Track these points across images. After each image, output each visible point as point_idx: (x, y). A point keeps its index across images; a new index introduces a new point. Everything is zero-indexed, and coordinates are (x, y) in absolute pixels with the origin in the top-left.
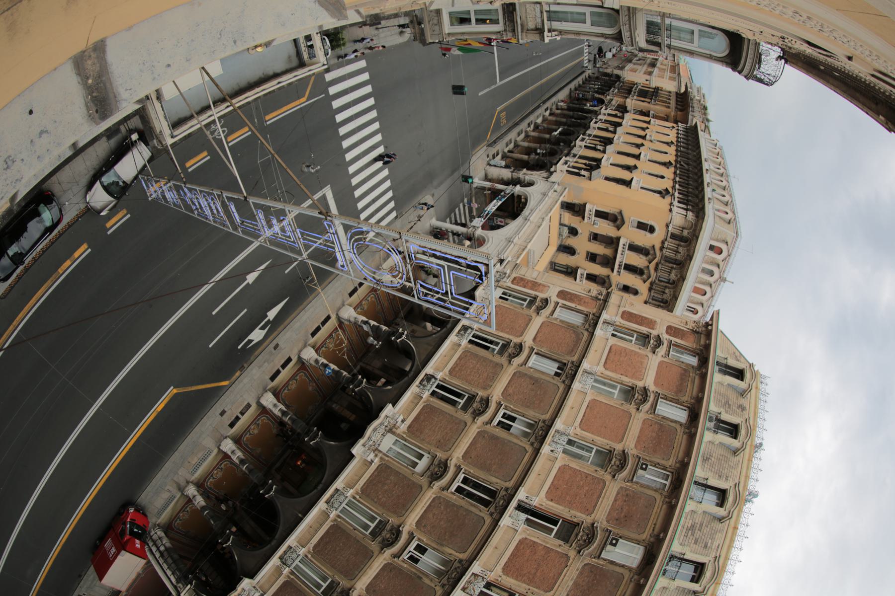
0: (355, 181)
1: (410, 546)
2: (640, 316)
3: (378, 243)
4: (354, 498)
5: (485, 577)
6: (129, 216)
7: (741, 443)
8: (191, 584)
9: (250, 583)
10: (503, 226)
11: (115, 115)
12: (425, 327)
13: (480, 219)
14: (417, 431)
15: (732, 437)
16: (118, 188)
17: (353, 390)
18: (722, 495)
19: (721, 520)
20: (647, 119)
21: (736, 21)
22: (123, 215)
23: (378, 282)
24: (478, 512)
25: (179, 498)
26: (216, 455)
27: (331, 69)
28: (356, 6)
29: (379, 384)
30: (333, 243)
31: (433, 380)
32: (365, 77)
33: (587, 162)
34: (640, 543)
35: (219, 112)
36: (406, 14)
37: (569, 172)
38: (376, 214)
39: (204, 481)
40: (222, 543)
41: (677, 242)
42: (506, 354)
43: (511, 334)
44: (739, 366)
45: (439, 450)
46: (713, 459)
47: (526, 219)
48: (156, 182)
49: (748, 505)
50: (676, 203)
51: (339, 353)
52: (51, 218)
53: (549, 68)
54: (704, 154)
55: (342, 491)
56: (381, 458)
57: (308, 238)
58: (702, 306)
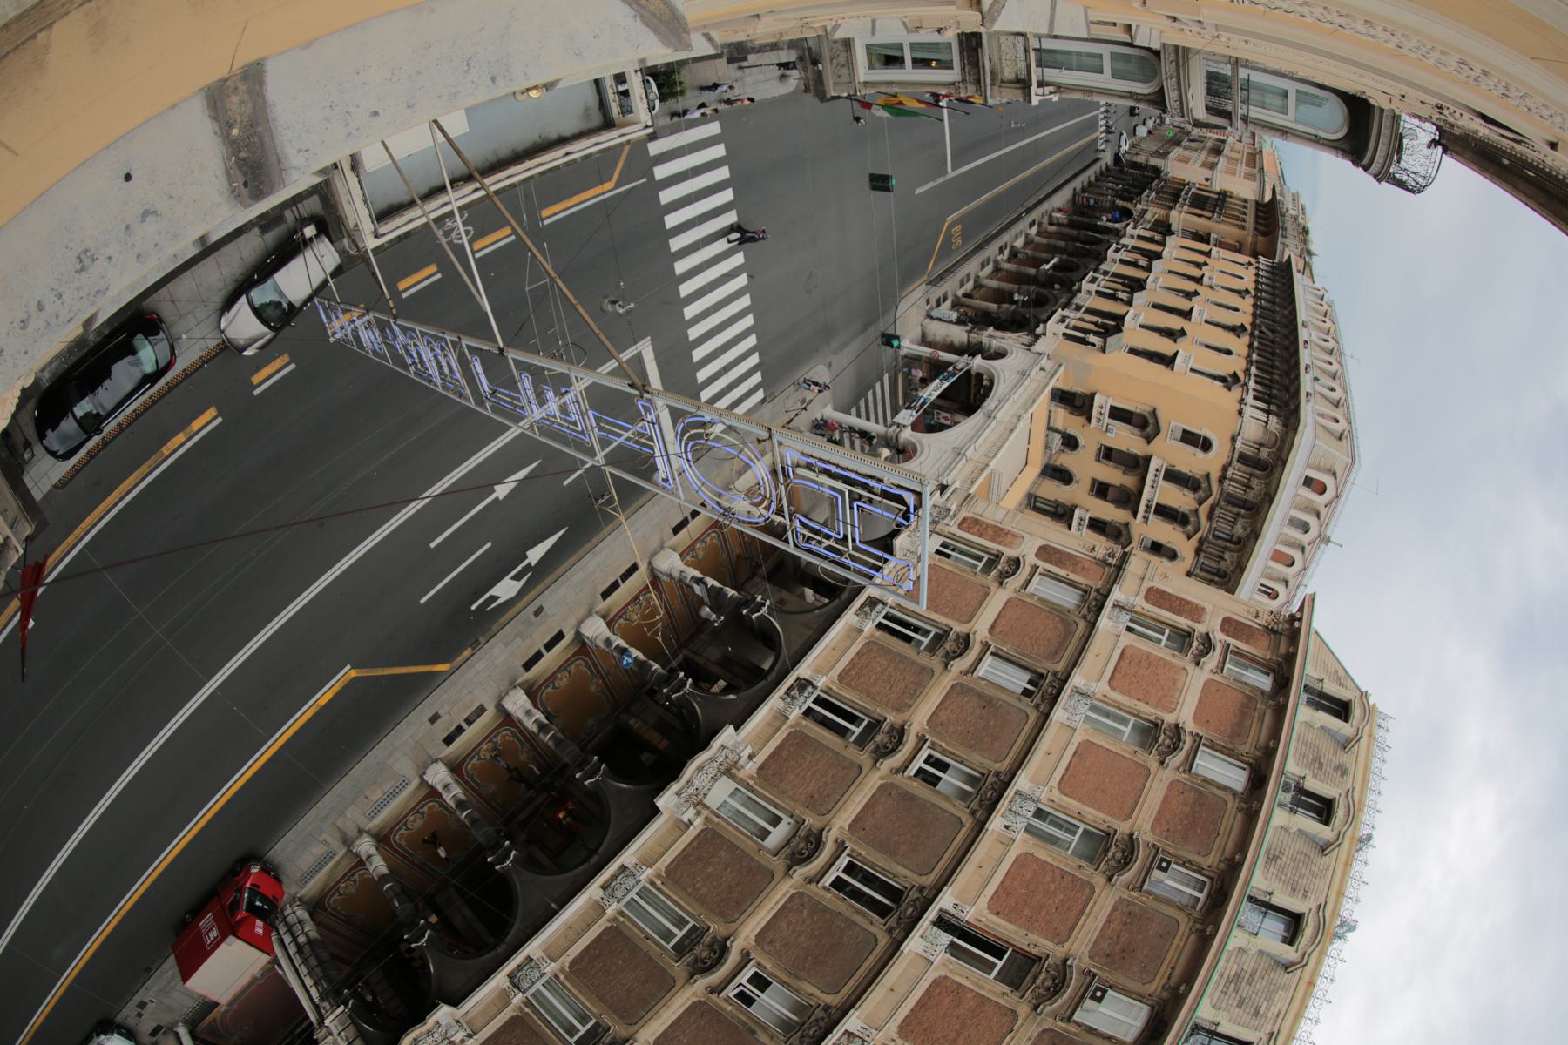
0: (694, 333)
1: (741, 974)
2: (1178, 598)
3: (733, 445)
4: (652, 883)
5: (867, 1039)
6: (293, 366)
7: (1335, 832)
8: (346, 1006)
9: (452, 1014)
10: (949, 427)
11: (278, 193)
12: (802, 596)
13: (909, 411)
14: (774, 775)
15: (1321, 822)
16: (278, 312)
17: (668, 697)
18: (1294, 923)
19: (1287, 967)
20: (1204, 247)
21: (1360, 76)
22: (283, 363)
23: (727, 512)
24: (866, 926)
25: (343, 857)
26: (416, 789)
27: (658, 133)
28: (705, 27)
29: (715, 689)
30: (651, 439)
31: (810, 689)
32: (719, 151)
33: (1100, 320)
34: (1145, 1000)
35: (460, 198)
36: (792, 45)
37: (1067, 337)
38: (728, 392)
39: (390, 832)
40: (409, 941)
41: (1249, 470)
42: (941, 652)
43: (951, 617)
44: (1343, 694)
45: (809, 812)
46: (1284, 859)
47: (990, 417)
48: (345, 311)
49: (1337, 943)
50: (1250, 399)
51: (649, 631)
52: (154, 359)
53: (1037, 151)
54: (1302, 314)
55: (632, 869)
56: (707, 818)
57: (607, 427)
58: (1287, 586)
